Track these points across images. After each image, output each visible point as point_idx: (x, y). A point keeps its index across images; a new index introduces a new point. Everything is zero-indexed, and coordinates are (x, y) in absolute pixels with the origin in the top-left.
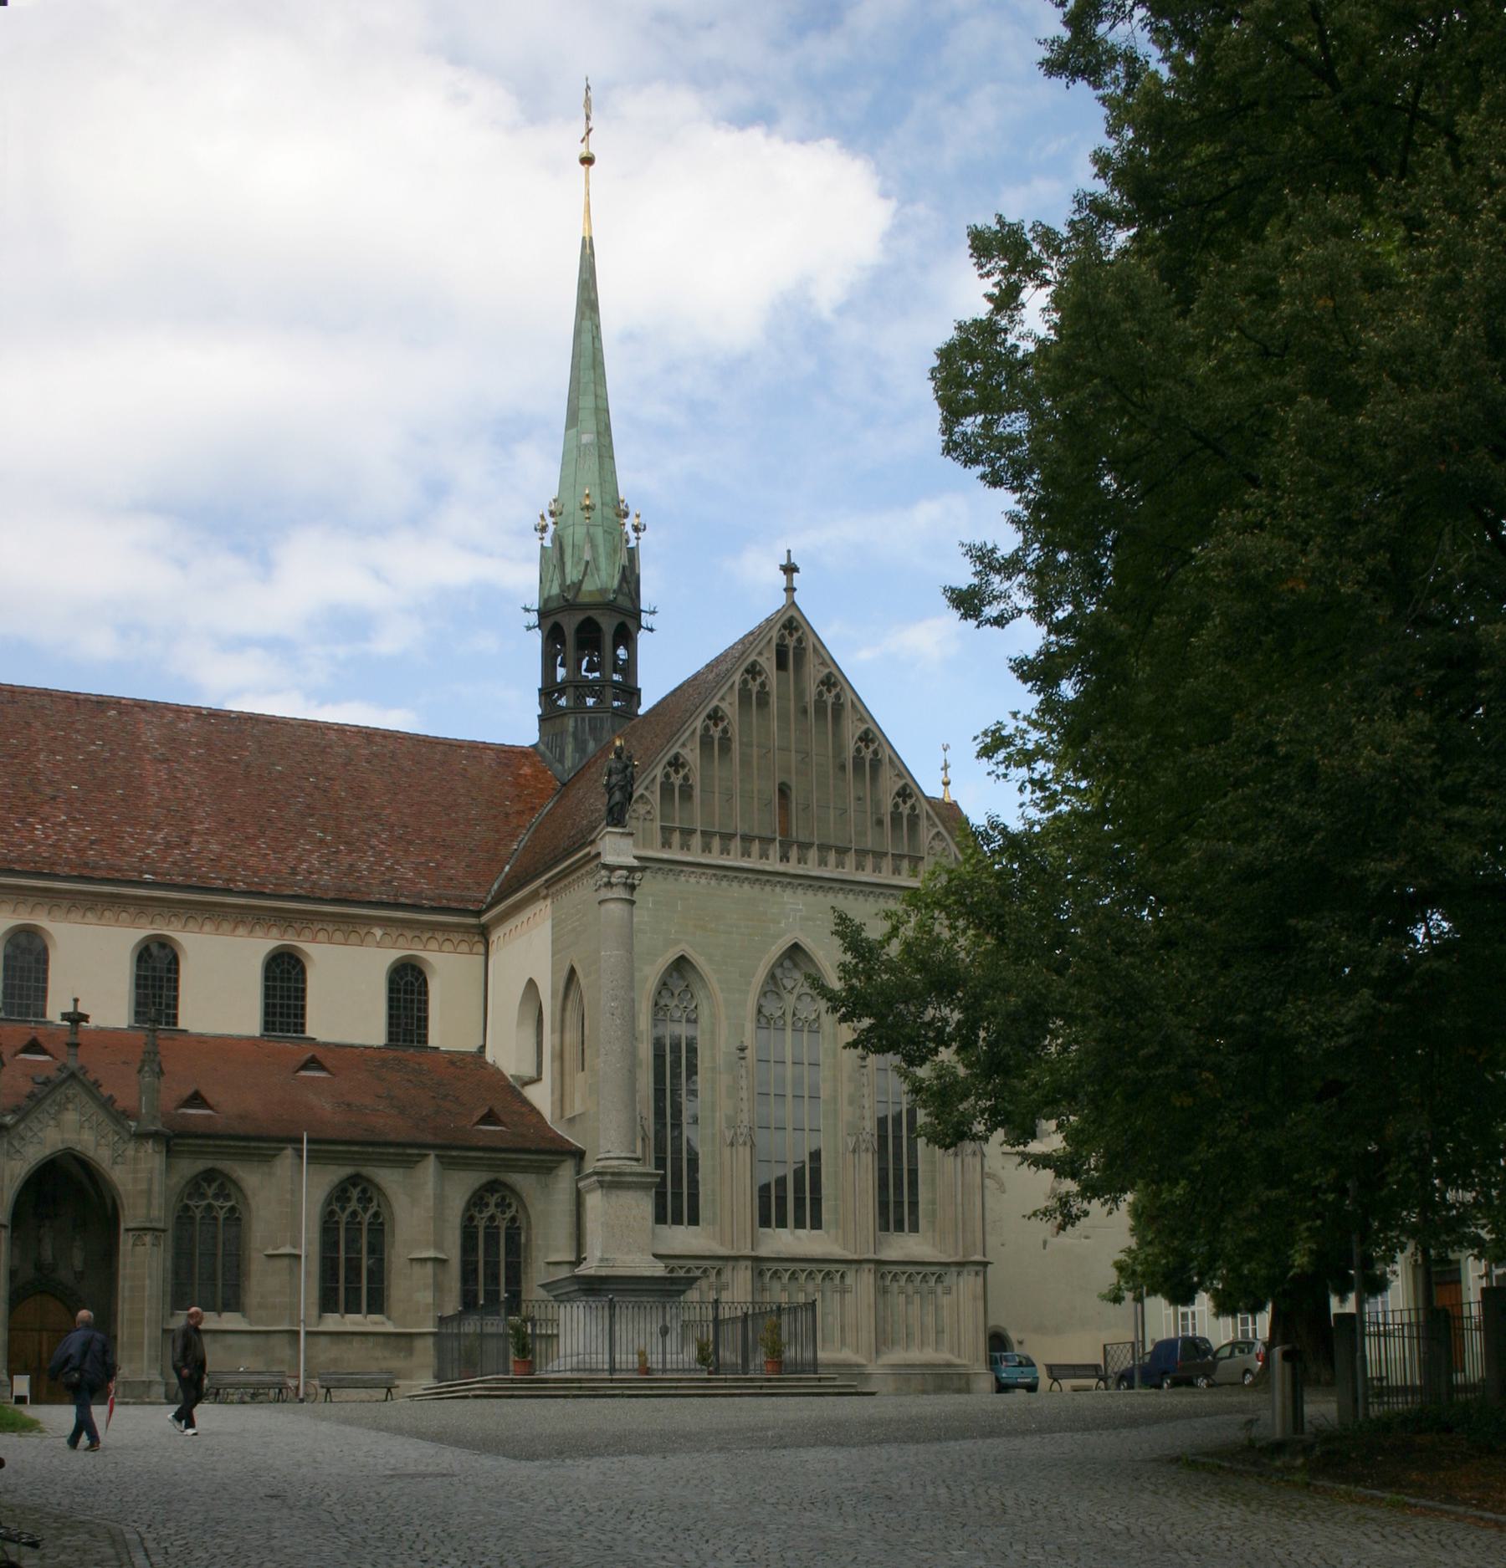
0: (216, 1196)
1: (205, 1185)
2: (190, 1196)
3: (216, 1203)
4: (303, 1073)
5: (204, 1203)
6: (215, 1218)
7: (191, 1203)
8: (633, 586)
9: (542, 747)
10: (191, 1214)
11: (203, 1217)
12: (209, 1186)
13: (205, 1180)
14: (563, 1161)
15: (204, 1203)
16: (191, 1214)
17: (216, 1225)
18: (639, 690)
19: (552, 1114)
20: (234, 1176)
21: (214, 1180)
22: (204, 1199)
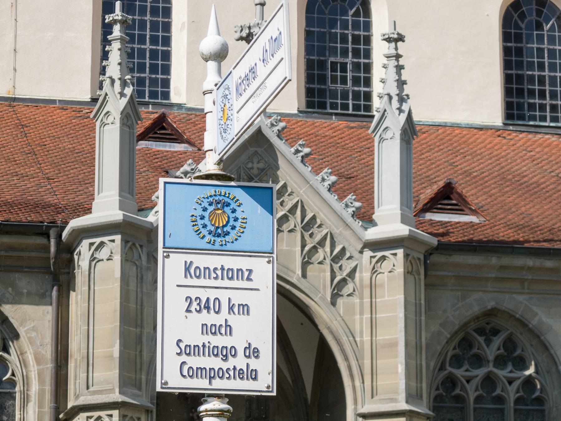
0: (500, 362)
1: (481, 339)
2: (457, 361)
3: (502, 373)
4: (429, 216)
5: (481, 372)
6: (500, 400)
7: (459, 373)
8: (244, 157)
9: (121, 199)
10: (457, 391)
11: (478, 399)
12: (488, 342)
13: (481, 331)
14: (453, 255)
15: (481, 372)
16: (457, 391)
17: (502, 411)
18: (401, 130)
19: (66, 236)
20: (534, 322)
21: (496, 332)
22: (480, 366)
